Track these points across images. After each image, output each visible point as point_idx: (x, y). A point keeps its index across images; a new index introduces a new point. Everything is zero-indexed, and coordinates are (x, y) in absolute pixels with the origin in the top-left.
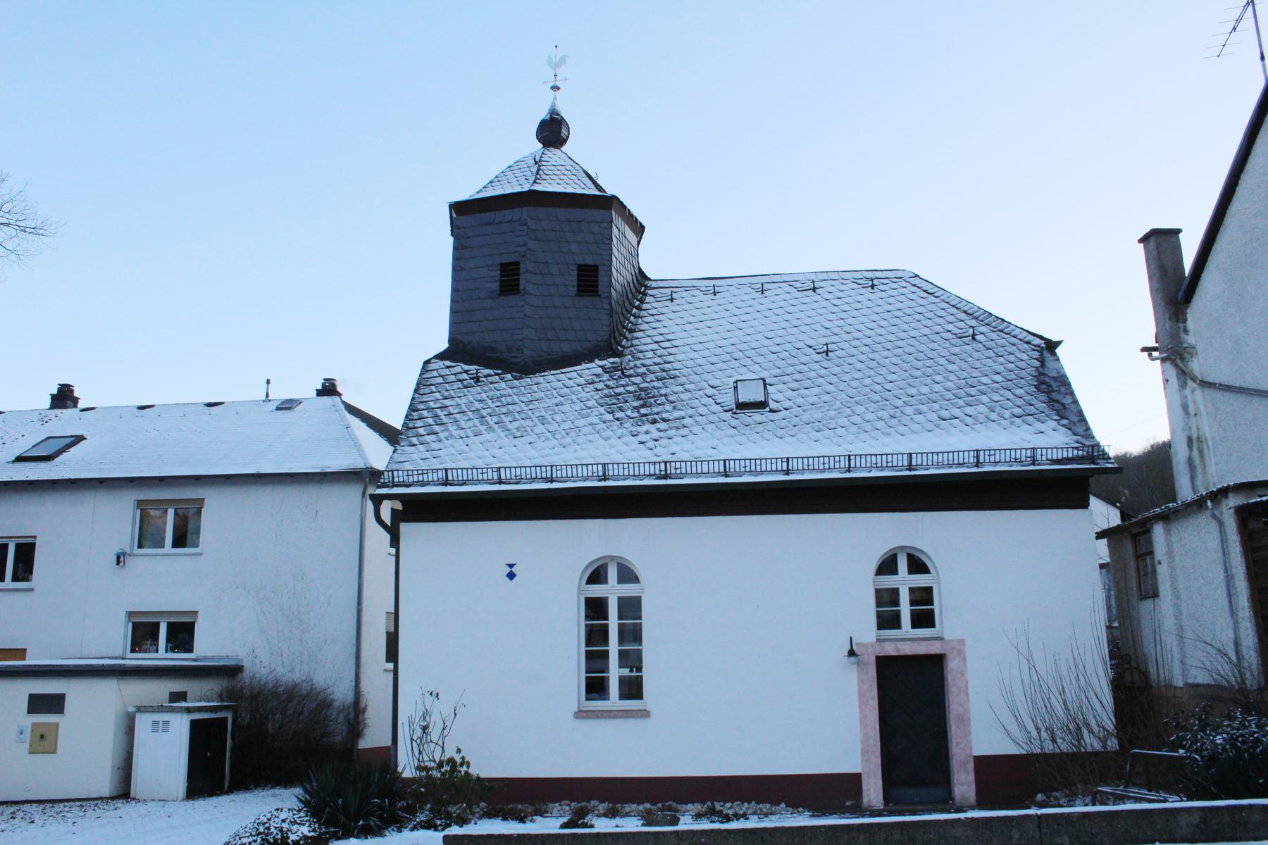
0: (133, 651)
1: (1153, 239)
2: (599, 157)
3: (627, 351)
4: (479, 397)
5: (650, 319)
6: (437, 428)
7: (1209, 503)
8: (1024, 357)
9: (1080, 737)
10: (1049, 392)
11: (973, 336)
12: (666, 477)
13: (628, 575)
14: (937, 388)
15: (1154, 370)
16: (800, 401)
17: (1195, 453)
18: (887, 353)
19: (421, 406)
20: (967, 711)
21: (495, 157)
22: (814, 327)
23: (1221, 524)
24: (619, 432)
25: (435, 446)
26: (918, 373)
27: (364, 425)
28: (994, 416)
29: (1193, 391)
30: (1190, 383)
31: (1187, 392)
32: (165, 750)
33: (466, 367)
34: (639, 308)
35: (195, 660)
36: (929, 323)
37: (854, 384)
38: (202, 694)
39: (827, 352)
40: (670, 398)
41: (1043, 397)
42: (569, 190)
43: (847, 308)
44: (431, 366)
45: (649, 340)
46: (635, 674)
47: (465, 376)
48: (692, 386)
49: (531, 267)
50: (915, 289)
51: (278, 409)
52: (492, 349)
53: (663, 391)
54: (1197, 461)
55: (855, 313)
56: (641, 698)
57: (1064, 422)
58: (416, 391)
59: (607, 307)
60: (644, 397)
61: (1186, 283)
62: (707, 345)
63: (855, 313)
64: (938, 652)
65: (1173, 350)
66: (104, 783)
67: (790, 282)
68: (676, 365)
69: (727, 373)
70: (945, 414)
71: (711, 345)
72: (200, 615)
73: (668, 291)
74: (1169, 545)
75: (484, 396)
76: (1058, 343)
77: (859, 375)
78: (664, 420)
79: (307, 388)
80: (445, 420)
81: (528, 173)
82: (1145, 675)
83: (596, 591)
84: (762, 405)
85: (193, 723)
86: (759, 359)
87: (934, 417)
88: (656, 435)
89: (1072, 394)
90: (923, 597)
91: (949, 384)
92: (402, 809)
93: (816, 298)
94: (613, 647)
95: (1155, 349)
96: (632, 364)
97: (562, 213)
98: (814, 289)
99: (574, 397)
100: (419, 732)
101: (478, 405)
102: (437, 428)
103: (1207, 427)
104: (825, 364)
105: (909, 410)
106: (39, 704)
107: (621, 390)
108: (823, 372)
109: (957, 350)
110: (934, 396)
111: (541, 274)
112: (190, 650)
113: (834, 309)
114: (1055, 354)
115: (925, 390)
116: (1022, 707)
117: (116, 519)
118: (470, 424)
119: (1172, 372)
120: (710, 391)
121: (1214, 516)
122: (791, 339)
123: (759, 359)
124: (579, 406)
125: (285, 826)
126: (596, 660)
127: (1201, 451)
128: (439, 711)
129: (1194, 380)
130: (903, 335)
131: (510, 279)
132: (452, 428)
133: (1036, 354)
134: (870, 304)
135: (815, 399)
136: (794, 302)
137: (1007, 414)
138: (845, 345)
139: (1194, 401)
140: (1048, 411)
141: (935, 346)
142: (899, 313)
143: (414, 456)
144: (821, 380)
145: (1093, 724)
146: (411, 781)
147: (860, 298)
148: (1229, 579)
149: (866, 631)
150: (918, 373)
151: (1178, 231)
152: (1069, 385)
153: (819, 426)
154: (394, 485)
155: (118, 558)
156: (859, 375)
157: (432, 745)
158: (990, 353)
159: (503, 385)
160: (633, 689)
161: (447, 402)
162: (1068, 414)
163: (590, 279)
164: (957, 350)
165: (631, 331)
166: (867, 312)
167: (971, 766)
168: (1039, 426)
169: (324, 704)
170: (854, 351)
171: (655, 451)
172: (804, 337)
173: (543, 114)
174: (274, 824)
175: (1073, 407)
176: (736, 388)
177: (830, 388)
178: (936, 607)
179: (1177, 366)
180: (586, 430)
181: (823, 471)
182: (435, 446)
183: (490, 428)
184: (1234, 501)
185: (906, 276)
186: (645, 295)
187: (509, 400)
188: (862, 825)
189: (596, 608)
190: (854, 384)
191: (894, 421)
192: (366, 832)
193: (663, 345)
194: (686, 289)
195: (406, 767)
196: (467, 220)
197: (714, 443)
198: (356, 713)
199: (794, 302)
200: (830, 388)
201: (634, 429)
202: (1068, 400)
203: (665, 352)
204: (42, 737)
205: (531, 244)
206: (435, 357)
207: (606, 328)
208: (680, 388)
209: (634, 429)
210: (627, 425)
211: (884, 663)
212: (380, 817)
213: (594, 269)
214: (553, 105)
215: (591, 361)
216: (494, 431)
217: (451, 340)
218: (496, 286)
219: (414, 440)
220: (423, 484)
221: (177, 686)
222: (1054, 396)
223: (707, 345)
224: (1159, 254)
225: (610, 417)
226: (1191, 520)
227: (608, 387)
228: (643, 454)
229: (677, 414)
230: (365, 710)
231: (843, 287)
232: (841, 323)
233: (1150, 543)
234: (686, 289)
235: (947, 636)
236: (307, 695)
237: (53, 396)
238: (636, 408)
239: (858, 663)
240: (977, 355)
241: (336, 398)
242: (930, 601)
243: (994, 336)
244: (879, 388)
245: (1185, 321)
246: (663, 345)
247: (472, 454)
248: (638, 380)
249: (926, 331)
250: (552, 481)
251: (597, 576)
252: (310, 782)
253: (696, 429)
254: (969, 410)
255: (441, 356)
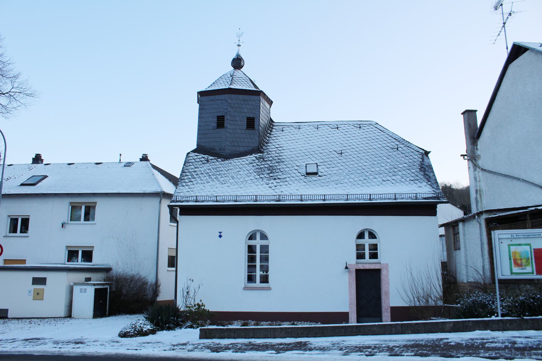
0: (68, 261)
1: (466, 114)
2: (258, 74)
3: (265, 151)
4: (208, 168)
5: (274, 138)
6: (193, 180)
7: (476, 217)
8: (416, 157)
9: (428, 301)
10: (424, 171)
11: (397, 148)
12: (279, 201)
13: (264, 237)
14: (382, 168)
15: (465, 163)
16: (330, 172)
17: (478, 196)
18: (364, 154)
19: (186, 171)
20: (388, 290)
21: (214, 73)
22: (337, 143)
23: (480, 224)
24: (262, 183)
25: (192, 186)
26: (375, 163)
27: (159, 173)
28: (403, 180)
29: (479, 172)
30: (477, 169)
31: (477, 172)
32: (85, 299)
33: (203, 156)
34: (270, 134)
35: (93, 265)
36: (380, 143)
37: (351, 166)
38: (97, 279)
39: (341, 154)
40: (281, 170)
41: (422, 173)
42: (244, 88)
43: (349, 136)
44: (190, 155)
45: (273, 147)
46: (265, 273)
47: (203, 159)
48: (290, 166)
49: (229, 117)
50: (376, 129)
51: (125, 166)
52: (213, 149)
53: (278, 167)
54: (479, 199)
55: (353, 138)
56: (268, 282)
57: (429, 183)
58: (184, 165)
59: (258, 134)
60: (271, 169)
61: (478, 130)
62: (296, 149)
63: (353, 138)
64: (379, 268)
65: (472, 157)
66: (62, 311)
67: (328, 125)
68: (284, 157)
69: (303, 161)
70: (385, 179)
71: (297, 149)
72: (95, 248)
73: (281, 127)
74: (464, 231)
75: (210, 167)
76: (430, 152)
77: (353, 163)
78: (279, 179)
79: (136, 158)
80: (196, 176)
81: (228, 80)
82: (455, 278)
83: (252, 242)
84: (316, 174)
85: (96, 290)
86: (315, 156)
87: (380, 180)
88: (276, 184)
89: (433, 172)
90: (374, 247)
91: (387, 167)
92: (181, 321)
93: (339, 132)
94: (258, 263)
95: (466, 155)
96: (267, 156)
97: (241, 97)
98: (337, 128)
99: (245, 169)
100: (185, 294)
101: (208, 171)
102: (193, 180)
103: (483, 186)
104: (340, 158)
105: (371, 177)
106: (36, 281)
107: (262, 166)
108: (339, 161)
109: (391, 154)
110: (381, 172)
111: (233, 120)
112: (91, 261)
113: (345, 136)
114: (427, 156)
115: (378, 169)
116: (408, 289)
117: (62, 209)
118: (205, 178)
119: (471, 165)
120: (296, 168)
121: (478, 221)
122: (328, 148)
123: (315, 156)
124: (246, 172)
125: (142, 325)
126: (251, 268)
127: (480, 195)
128: (193, 287)
129: (479, 168)
130: (371, 147)
131: (221, 122)
132: (198, 180)
133: (421, 156)
134: (358, 134)
135: (336, 172)
136: (330, 133)
137: (408, 179)
138: (348, 151)
139: (479, 176)
140: (423, 179)
141: (382, 152)
142: (369, 139)
143: (184, 190)
144: (338, 164)
145: (432, 296)
146: (184, 312)
147: (355, 132)
148: (482, 244)
149: (352, 260)
150: (375, 163)
151: (476, 111)
152: (432, 169)
153: (337, 182)
154: (177, 202)
155: (63, 225)
156: (353, 163)
157: (190, 299)
158: (403, 155)
159: (218, 163)
160: (265, 279)
161: (196, 170)
162: (431, 180)
163: (251, 123)
164: (391, 154)
165: (267, 143)
166: (357, 137)
167: (389, 310)
168: (420, 184)
169: (145, 283)
170: (352, 153)
171: (275, 190)
172: (332, 147)
173: (234, 56)
174: (138, 325)
175: (433, 178)
176: (306, 167)
177: (342, 168)
178: (378, 251)
179: (473, 163)
180: (249, 182)
181: (338, 200)
182: (192, 186)
183: (213, 180)
184: (484, 216)
185: (373, 123)
186: (272, 128)
187: (220, 169)
188: (343, 326)
189: (251, 249)
190: (351, 166)
191: (365, 181)
192: (169, 329)
193: (279, 149)
194: (288, 126)
195: (181, 305)
196: (205, 98)
197: (297, 188)
198: (156, 287)
199: (330, 133)
200: (342, 168)
201: (267, 182)
202: (431, 175)
203: (279, 152)
204: (38, 294)
205: (229, 109)
206: (191, 151)
207: (257, 142)
208: (285, 166)
209: (267, 182)
210: (265, 180)
211: (358, 271)
212: (173, 324)
213: (253, 119)
214: (238, 52)
215: (251, 155)
216: (214, 181)
217: (197, 145)
218: (215, 124)
219: (184, 184)
220: (188, 201)
221: (88, 275)
222: (427, 173)
223: (296, 149)
224: (468, 119)
225: (258, 177)
226: (471, 222)
227: (258, 165)
228: (270, 192)
229: (284, 176)
230: (159, 286)
231: (348, 128)
232: (347, 142)
233: (458, 229)
234: (288, 126)
235: (382, 262)
236: (139, 279)
237: (33, 159)
238: (268, 174)
239: (349, 271)
240: (398, 156)
241: (148, 162)
242: (376, 249)
243: (405, 148)
244: (360, 168)
245: (477, 145)
246: (279, 149)
247: (206, 190)
248: (269, 162)
249: (379, 146)
250: (236, 201)
251: (252, 237)
252: (149, 311)
253: (291, 182)
254: (394, 178)
255: (194, 151)
